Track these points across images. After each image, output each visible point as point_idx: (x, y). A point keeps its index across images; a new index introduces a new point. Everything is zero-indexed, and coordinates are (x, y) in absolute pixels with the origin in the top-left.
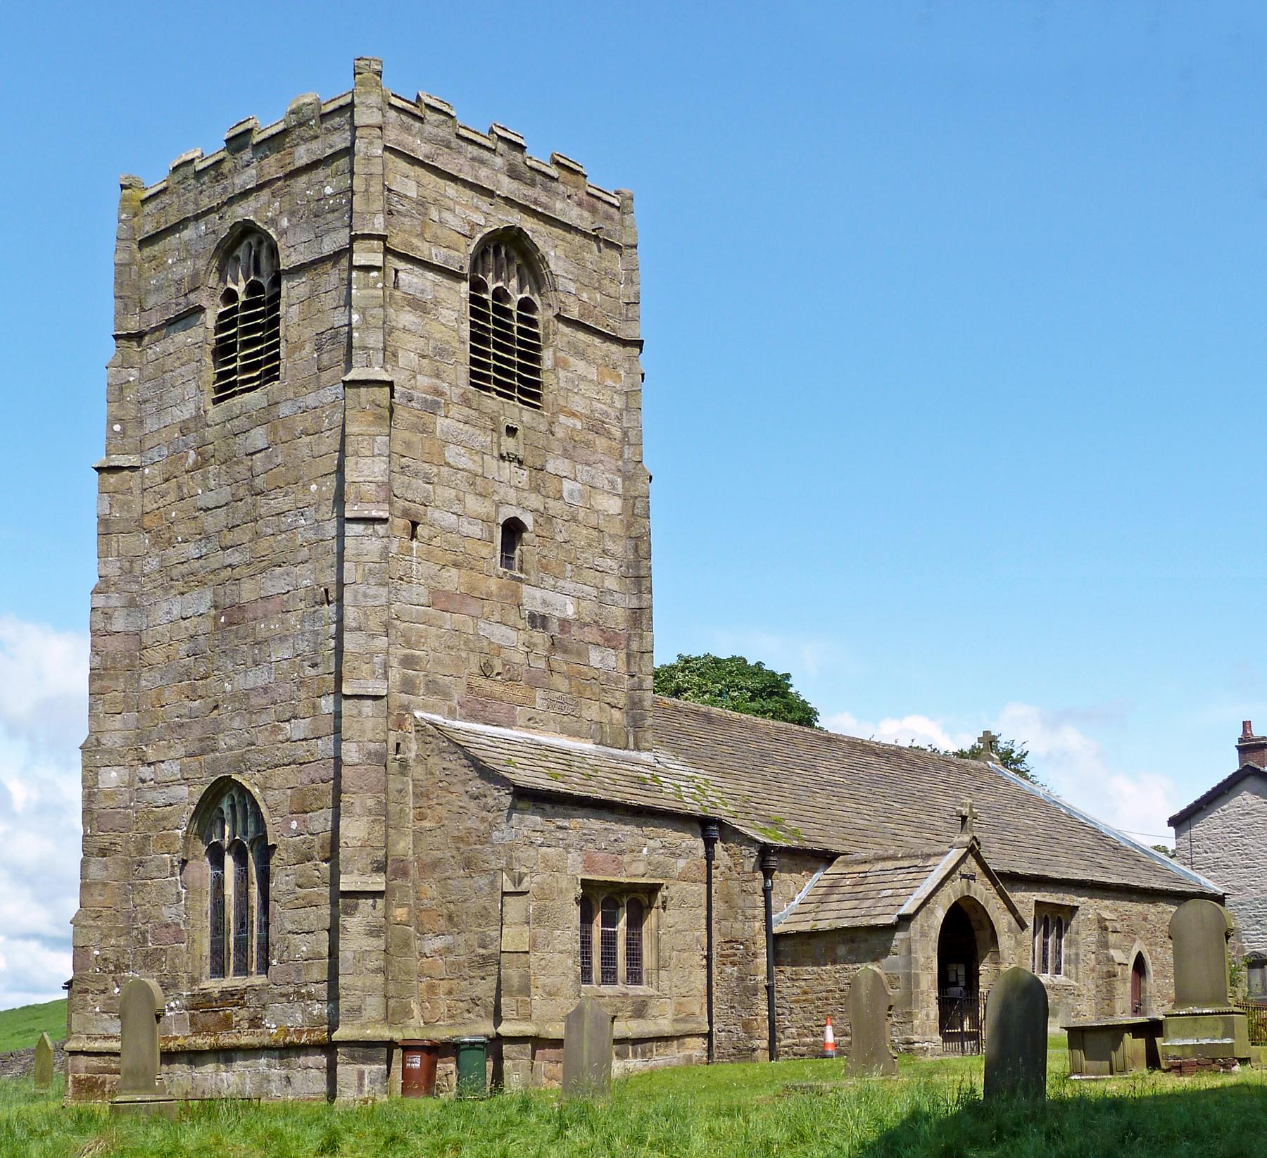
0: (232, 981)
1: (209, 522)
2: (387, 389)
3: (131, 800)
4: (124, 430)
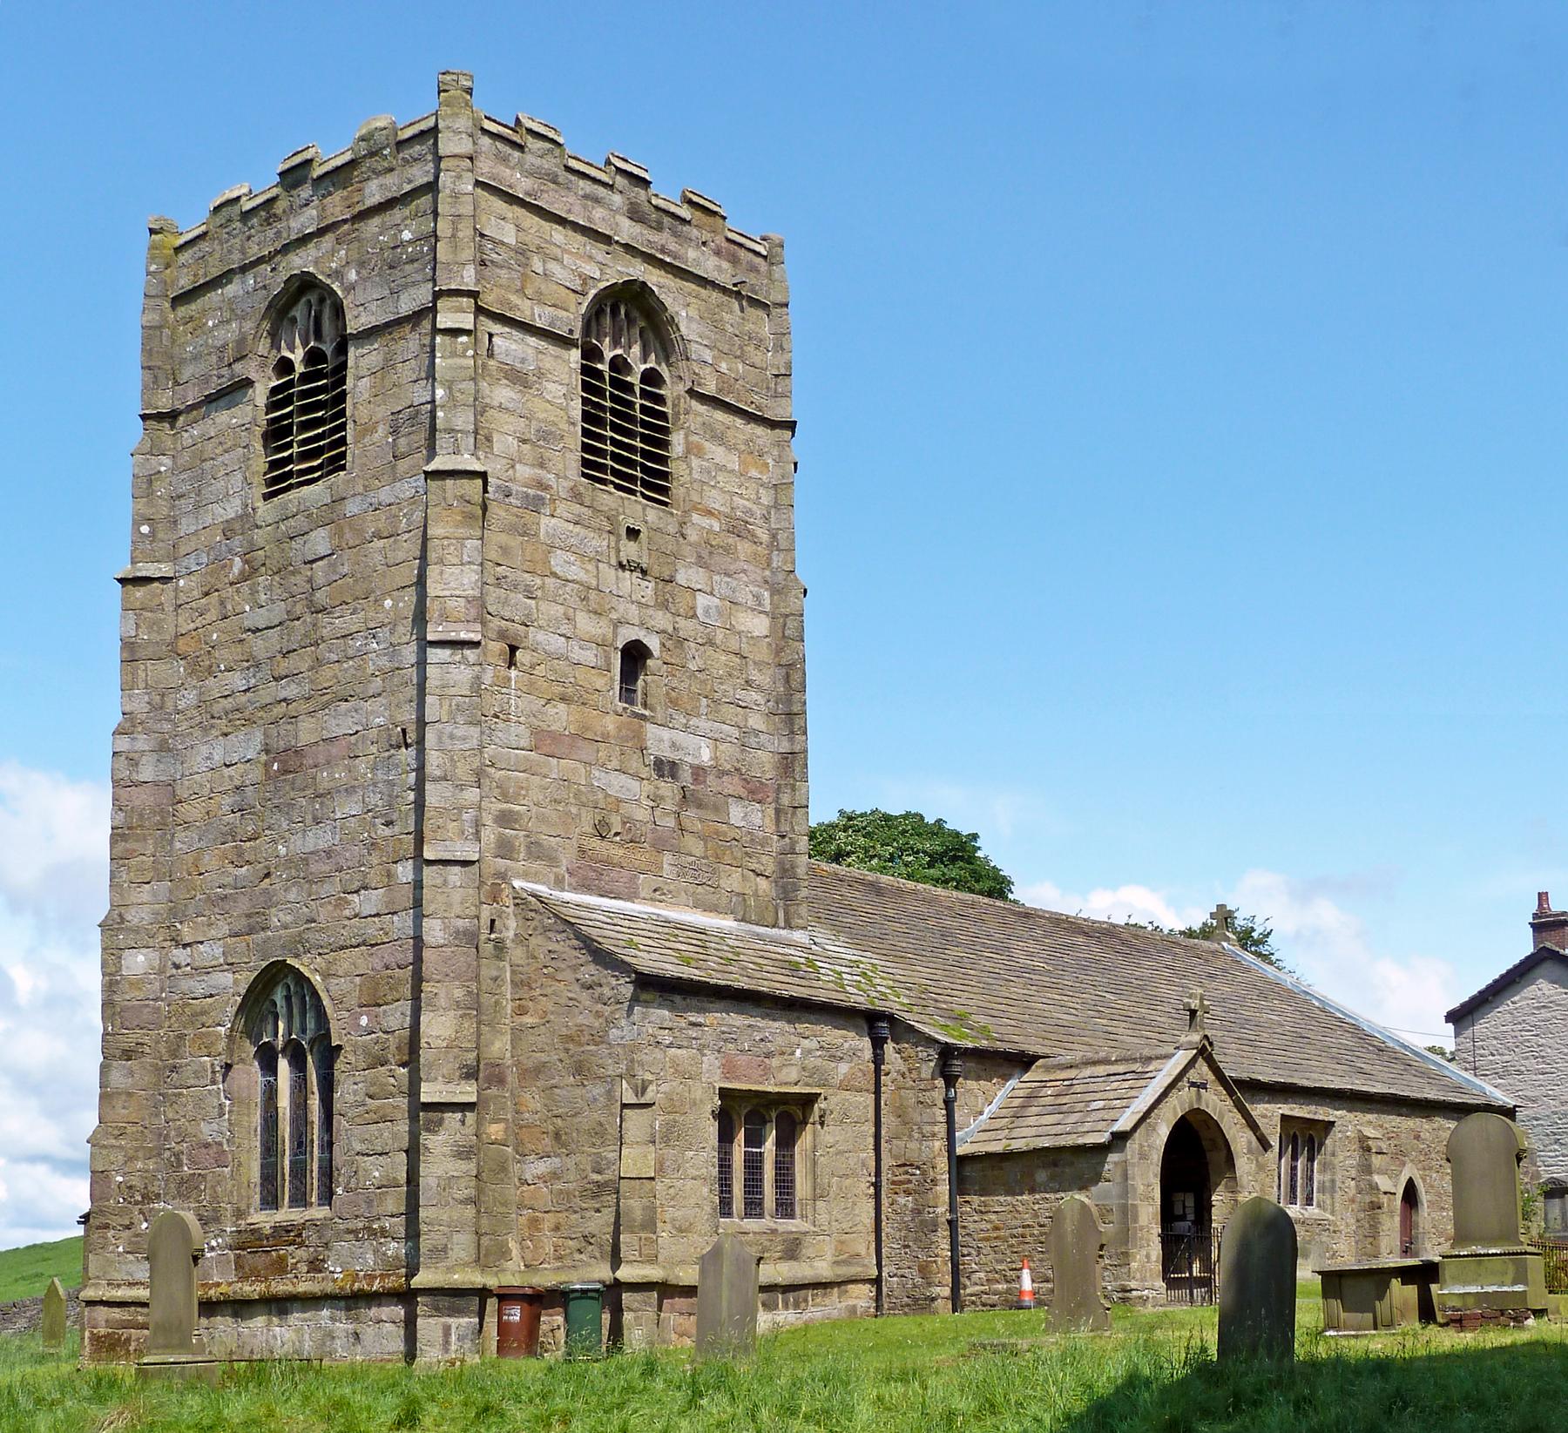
0: (287, 1214)
1: (259, 646)
2: (479, 482)
3: (162, 990)
4: (153, 533)
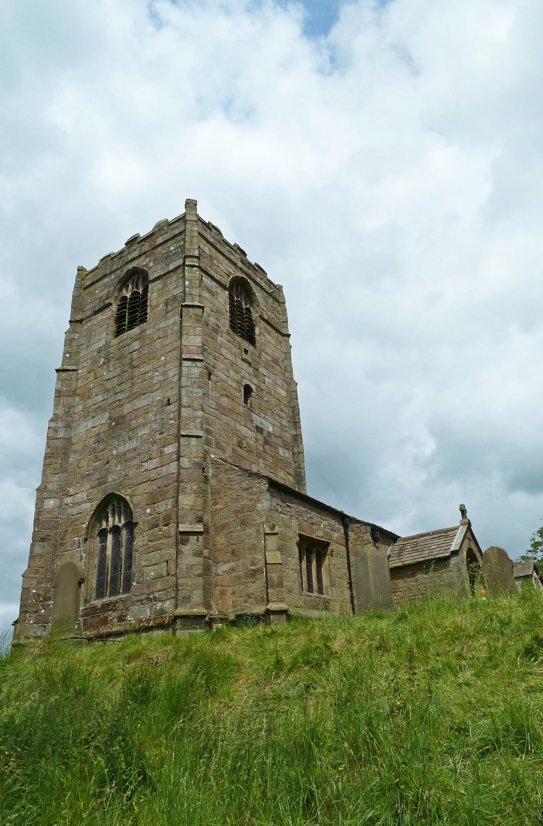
0: (106, 600)
1: (109, 385)
2: (201, 310)
3: (60, 514)
4: (70, 356)
